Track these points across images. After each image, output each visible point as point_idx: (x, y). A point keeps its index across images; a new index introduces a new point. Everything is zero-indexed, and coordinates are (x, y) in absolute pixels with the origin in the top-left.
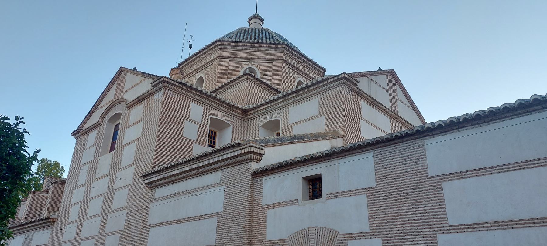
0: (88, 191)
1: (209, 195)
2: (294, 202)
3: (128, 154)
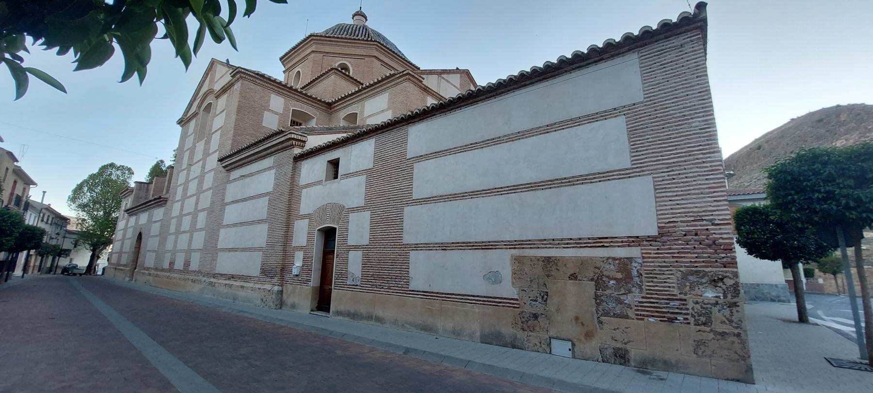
0: (188, 174)
1: (263, 177)
2: (319, 183)
3: (216, 139)
